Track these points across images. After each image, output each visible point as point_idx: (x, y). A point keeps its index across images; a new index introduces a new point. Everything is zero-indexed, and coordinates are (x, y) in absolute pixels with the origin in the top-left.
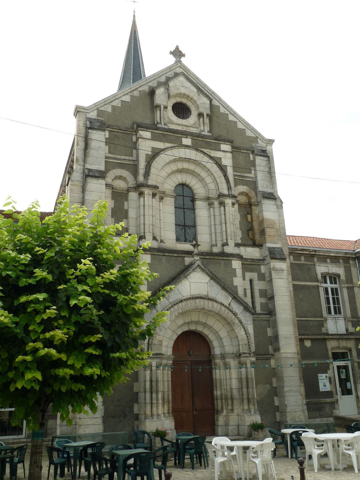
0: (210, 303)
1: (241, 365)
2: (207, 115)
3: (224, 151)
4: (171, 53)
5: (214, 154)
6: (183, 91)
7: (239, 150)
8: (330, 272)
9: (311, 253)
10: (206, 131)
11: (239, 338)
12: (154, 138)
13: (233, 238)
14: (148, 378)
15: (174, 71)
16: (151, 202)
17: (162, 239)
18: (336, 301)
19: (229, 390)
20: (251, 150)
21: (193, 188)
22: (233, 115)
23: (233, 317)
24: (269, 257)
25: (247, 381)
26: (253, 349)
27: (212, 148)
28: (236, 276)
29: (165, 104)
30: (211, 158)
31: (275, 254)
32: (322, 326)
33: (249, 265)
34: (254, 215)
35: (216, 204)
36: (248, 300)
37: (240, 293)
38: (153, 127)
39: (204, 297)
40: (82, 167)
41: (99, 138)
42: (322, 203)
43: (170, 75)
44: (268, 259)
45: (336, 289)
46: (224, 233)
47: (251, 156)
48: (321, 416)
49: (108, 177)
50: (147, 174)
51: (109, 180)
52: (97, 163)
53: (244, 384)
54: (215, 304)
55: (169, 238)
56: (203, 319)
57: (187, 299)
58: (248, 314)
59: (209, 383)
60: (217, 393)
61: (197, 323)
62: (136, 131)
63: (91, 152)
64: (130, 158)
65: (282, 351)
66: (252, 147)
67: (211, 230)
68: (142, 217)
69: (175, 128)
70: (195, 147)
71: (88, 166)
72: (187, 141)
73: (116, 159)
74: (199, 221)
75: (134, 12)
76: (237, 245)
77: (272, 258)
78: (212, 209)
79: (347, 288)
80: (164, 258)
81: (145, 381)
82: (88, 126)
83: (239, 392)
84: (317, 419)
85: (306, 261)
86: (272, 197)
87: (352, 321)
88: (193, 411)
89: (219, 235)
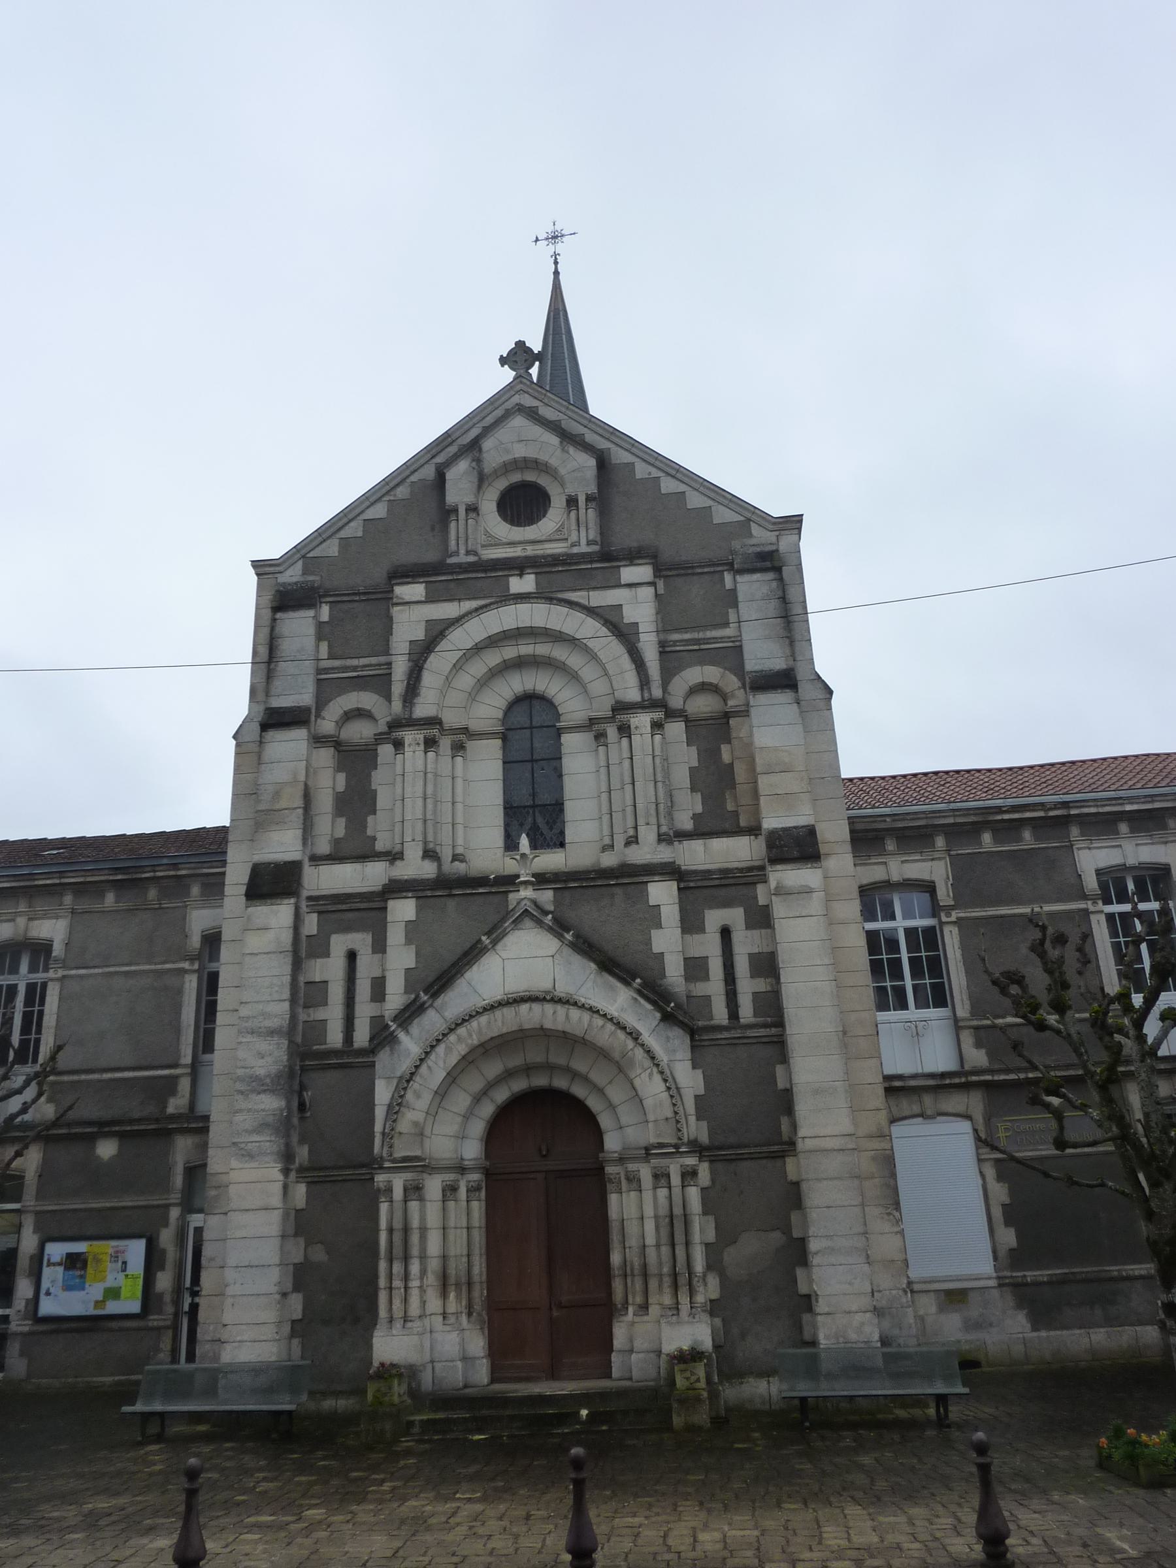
0: (561, 1010)
3: (630, 585)
5: (598, 598)
7: (690, 571)
8: (1131, 861)
9: (1051, 814)
11: (648, 1103)
12: (430, 599)
13: (653, 820)
17: (459, 850)
18: (936, 966)
21: (556, 702)
22: (673, 477)
23: (630, 1044)
27: (594, 584)
28: (659, 926)
30: (591, 611)
31: (800, 847)
35: (612, 732)
39: (542, 995)
42: (927, 669)
48: (1111, 1321)
49: (324, 719)
52: (296, 692)
54: (575, 1013)
55: (484, 845)
57: (491, 1008)
59: (599, 1229)
61: (528, 1069)
69: (504, 555)
70: (542, 595)
72: (524, 584)
74: (570, 786)
75: (556, 263)
80: (451, 904)
84: (1097, 1330)
85: (1037, 839)
88: (551, 1309)
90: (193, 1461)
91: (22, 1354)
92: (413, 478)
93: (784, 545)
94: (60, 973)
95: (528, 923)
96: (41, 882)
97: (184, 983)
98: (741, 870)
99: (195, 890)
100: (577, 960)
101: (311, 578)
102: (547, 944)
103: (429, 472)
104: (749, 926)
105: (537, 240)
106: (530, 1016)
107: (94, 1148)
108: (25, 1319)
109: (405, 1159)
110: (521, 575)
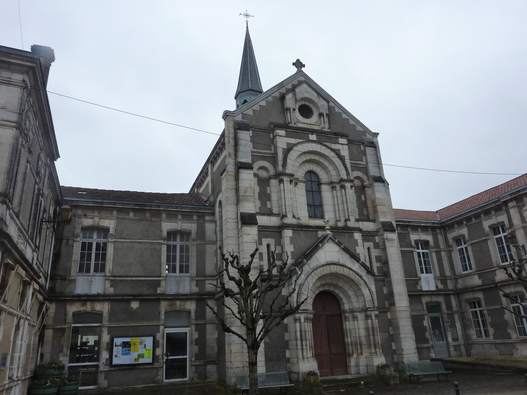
1: (367, 317)
2: (327, 115)
3: (342, 144)
4: (294, 64)
5: (334, 146)
6: (306, 95)
8: (422, 239)
10: (326, 128)
11: (365, 296)
12: (287, 136)
14: (298, 329)
15: (298, 79)
16: (289, 188)
19: (358, 338)
20: (364, 142)
23: (360, 279)
24: (382, 229)
25: (373, 330)
26: (376, 304)
29: (293, 107)
30: (332, 150)
31: (388, 227)
32: (417, 284)
33: (367, 236)
34: (367, 195)
35: (338, 187)
36: (368, 264)
37: (362, 259)
38: (285, 126)
40: (233, 160)
41: (245, 136)
43: (295, 82)
44: (381, 231)
45: (427, 253)
46: (346, 211)
47: (362, 147)
50: (284, 165)
51: (255, 170)
53: (371, 332)
54: (345, 269)
56: (335, 282)
57: (323, 266)
58: (370, 277)
59: (342, 333)
60: (348, 340)
61: (329, 285)
62: (273, 131)
63: (241, 148)
64: (270, 152)
65: (397, 305)
66: (362, 140)
67: (335, 208)
68: (283, 200)
71: (240, 160)
72: (313, 137)
73: (259, 153)
75: (247, 24)
76: (357, 220)
77: (385, 231)
78: (334, 191)
79: (436, 252)
80: (302, 233)
81: (296, 332)
82: (237, 127)
83: (366, 339)
85: (401, 230)
86: (381, 180)
87: (440, 280)
89: (341, 212)
90: (456, 382)
91: (105, 378)
92: (273, 95)
93: (374, 140)
94: (113, 240)
95: (330, 241)
96: (106, 206)
97: (161, 248)
98: (372, 232)
99: (164, 215)
100: (344, 253)
101: (245, 121)
102: (336, 248)
103: (277, 94)
104: (375, 248)
105: (247, 15)
106: (334, 269)
107: (130, 304)
108: (106, 365)
109: (304, 310)
110: (312, 134)
